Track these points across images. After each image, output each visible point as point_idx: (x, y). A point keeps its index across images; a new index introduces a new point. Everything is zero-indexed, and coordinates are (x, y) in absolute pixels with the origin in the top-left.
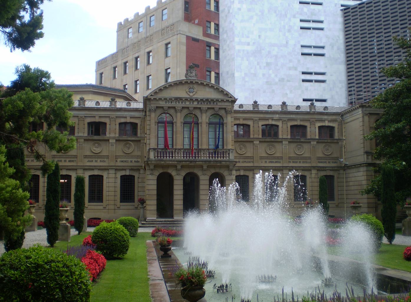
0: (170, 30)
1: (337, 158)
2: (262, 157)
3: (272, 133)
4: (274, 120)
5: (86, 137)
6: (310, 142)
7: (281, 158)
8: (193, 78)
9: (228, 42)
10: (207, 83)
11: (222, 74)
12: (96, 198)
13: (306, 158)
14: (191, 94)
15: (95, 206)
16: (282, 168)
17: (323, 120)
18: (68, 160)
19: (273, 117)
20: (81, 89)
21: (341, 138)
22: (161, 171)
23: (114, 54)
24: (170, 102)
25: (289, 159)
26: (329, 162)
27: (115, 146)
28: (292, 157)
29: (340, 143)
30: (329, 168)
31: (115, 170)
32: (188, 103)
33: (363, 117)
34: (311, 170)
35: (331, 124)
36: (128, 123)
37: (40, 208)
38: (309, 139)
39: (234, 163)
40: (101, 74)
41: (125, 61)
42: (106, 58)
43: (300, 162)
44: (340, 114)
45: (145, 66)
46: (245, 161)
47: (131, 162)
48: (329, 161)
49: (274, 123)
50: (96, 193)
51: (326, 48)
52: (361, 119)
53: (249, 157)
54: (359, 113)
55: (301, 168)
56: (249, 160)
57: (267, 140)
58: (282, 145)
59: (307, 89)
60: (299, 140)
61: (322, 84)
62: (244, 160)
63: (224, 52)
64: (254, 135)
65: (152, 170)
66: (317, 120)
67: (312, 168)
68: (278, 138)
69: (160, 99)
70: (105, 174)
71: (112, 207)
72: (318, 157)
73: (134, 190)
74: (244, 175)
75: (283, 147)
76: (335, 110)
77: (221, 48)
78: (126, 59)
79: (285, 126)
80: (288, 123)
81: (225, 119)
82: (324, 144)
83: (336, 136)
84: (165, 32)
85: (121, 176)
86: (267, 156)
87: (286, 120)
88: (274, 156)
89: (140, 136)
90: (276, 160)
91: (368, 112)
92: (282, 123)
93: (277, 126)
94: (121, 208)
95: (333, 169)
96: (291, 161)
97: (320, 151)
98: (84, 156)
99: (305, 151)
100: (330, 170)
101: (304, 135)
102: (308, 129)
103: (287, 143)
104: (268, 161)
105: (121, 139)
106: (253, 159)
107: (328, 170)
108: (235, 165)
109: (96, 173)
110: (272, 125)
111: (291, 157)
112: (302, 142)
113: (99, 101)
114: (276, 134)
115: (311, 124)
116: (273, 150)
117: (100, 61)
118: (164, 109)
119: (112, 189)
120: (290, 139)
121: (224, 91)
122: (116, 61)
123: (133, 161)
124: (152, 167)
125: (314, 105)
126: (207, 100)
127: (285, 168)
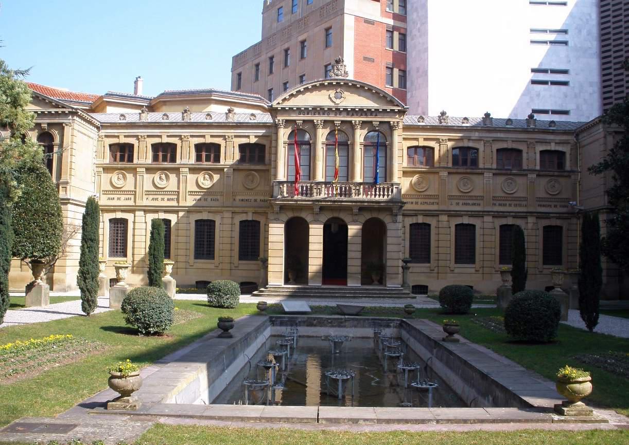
0: (331, 8)
1: (568, 200)
4: (472, 140)
6: (526, 175)
7: (482, 198)
8: (340, 77)
9: (419, 25)
10: (361, 84)
11: (409, 71)
12: (205, 252)
14: (338, 101)
16: (481, 213)
17: (548, 141)
18: (166, 197)
20: (198, 97)
21: (574, 169)
22: (290, 215)
23: (256, 45)
24: (306, 114)
25: (493, 200)
26: (555, 206)
27: (232, 178)
28: (498, 197)
29: (573, 177)
30: (555, 215)
33: (605, 137)
34: (527, 218)
35: (560, 148)
36: (421, 147)
37: (432, 272)
38: (524, 170)
39: (400, 204)
40: (240, 75)
41: (270, 55)
42: (245, 51)
43: (510, 205)
44: (574, 133)
45: (297, 61)
46: (425, 203)
47: (417, 203)
48: (556, 203)
49: (471, 144)
50: (205, 246)
51: (570, 32)
52: (602, 141)
54: (599, 131)
55: (512, 214)
56: (432, 201)
57: (460, 171)
58: (484, 179)
59: (538, 95)
60: (509, 172)
61: (563, 88)
63: (412, 39)
64: (484, 164)
65: (277, 213)
66: (539, 142)
67: (528, 214)
69: (291, 109)
70: (217, 219)
72: (537, 198)
73: (259, 243)
74: (253, 221)
75: (485, 182)
76: (570, 126)
77: (408, 33)
78: (271, 52)
79: (488, 150)
80: (493, 146)
81: (389, 138)
82: (547, 179)
83: (568, 166)
84: (325, 11)
85: (241, 222)
86: (111, 189)
87: (533, 142)
89: (438, 166)
91: (613, 130)
92: (484, 146)
94: (195, 267)
95: (560, 216)
96: (497, 203)
97: (542, 186)
99: (520, 187)
100: (557, 218)
101: (519, 164)
102: (525, 155)
103: (491, 175)
104: (461, 202)
105: (241, 167)
106: (178, 195)
107: (553, 217)
108: (401, 207)
109: (466, 220)
110: (469, 148)
111: (496, 197)
112: (514, 175)
114: (475, 162)
115: (528, 147)
116: (469, 186)
117: (237, 56)
118: (296, 123)
119: (228, 240)
120: (496, 169)
121: (386, 95)
122: (259, 55)
123: (258, 200)
124: (277, 209)
125: (491, 117)
126: (361, 110)
127: (486, 213)
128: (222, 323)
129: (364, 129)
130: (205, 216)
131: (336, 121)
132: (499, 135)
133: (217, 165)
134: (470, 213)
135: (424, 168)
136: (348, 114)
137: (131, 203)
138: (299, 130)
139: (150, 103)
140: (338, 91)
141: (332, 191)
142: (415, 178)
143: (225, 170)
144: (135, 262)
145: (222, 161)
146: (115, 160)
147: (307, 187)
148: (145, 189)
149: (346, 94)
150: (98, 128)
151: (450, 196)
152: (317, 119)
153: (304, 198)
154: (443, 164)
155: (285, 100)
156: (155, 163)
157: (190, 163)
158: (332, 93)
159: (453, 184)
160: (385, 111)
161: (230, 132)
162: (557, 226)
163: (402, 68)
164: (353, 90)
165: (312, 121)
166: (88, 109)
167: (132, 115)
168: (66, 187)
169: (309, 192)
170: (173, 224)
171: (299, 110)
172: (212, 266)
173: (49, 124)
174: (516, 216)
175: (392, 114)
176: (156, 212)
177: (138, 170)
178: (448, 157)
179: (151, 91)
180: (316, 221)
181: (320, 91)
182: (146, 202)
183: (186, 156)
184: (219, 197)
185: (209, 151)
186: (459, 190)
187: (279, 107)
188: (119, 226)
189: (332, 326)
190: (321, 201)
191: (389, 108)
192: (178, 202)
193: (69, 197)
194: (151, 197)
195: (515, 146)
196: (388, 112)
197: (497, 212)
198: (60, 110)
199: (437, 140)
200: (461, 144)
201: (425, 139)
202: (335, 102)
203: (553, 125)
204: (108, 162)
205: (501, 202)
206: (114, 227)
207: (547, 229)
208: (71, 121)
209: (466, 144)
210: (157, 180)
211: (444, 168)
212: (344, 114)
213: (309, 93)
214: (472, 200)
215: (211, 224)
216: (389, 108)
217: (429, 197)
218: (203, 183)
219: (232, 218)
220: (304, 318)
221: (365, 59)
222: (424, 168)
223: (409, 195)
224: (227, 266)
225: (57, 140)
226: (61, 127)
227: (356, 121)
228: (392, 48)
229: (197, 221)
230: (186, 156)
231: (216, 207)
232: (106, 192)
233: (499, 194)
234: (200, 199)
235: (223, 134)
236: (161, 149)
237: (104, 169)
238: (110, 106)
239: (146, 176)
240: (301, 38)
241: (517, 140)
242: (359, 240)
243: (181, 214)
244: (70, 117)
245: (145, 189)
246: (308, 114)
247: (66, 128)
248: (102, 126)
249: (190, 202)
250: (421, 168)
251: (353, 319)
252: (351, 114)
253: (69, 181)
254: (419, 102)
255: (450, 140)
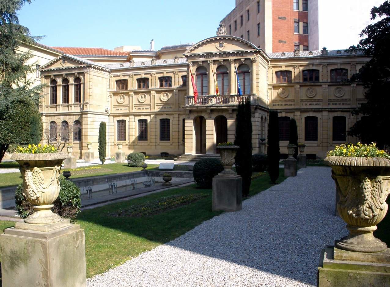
2: (302, 100)
3: (314, 77)
4: (315, 65)
5: (329, 82)
7: (321, 100)
8: (222, 35)
13: (345, 100)
14: (221, 49)
15: (308, 144)
18: (145, 107)
19: (313, 63)
22: (196, 115)
23: (234, 9)
31: (179, 114)
32: (218, 57)
41: (234, 20)
43: (340, 104)
47: (282, 105)
49: (314, 68)
50: (166, 133)
53: (291, 100)
55: (340, 110)
56: (291, 103)
62: (286, 103)
63: (311, 3)
68: (319, 82)
69: (195, 55)
71: (154, 144)
79: (325, 71)
81: (250, 68)
86: (118, 104)
88: (343, 98)
90: (317, 103)
93: (318, 71)
98: (300, 100)
103: (327, 86)
104: (308, 103)
105: (182, 89)
106: (151, 106)
109: (311, 114)
110: (313, 70)
113: (166, 60)
114: (317, 79)
115: (351, 67)
119: (177, 130)
125: (326, 50)
126: (233, 53)
128: (66, 174)
129: (215, 65)
130: (164, 117)
131: (200, 61)
132: (332, 61)
133: (170, 89)
134: (313, 110)
135: (285, 84)
136: (226, 56)
137: (127, 111)
138: (242, 64)
139: (157, 54)
140: (221, 42)
141: (219, 100)
142: (280, 90)
143: (174, 91)
144: (130, 143)
145: (173, 86)
146: (119, 89)
147: (203, 99)
148: (134, 104)
149: (225, 44)
150: (109, 72)
151: (329, 99)
152: (210, 60)
153: (201, 105)
154: (297, 81)
155: (191, 50)
156: (139, 89)
157: (156, 88)
158: (217, 44)
159: (304, 93)
160: (247, 52)
161: (176, 70)
162: (167, 119)
163: (305, 21)
164: (229, 41)
165: (207, 61)
166: (127, 60)
167: (148, 62)
168: (87, 105)
169: (204, 102)
170: (148, 121)
171: (199, 56)
172: (169, 144)
173: (78, 73)
174: (315, 111)
175: (246, 54)
176: (140, 115)
177: (130, 93)
178: (300, 76)
179: (156, 48)
180: (210, 118)
181: (206, 45)
182: (135, 110)
183: (155, 84)
184: (172, 106)
185: (165, 81)
186: (307, 96)
187: (189, 55)
188: (122, 124)
189: (177, 177)
190: (210, 107)
191: (249, 50)
192: (151, 110)
193: (88, 110)
194: (137, 108)
195: (342, 67)
196: (249, 53)
197: (331, 109)
198: (82, 66)
199: (293, 66)
200: (308, 68)
201: (286, 66)
202: (218, 49)
203: (339, 53)
204: (115, 90)
205: (333, 103)
206: (141, 124)
207: (335, 119)
208: (88, 71)
209: (311, 68)
210: (162, 97)
211: (297, 83)
212: (224, 55)
213: (205, 46)
214: (315, 102)
215: (168, 121)
216: (249, 50)
217: (290, 101)
218: (163, 99)
219: (179, 117)
220: (163, 172)
221: (280, 18)
222: (285, 84)
223: (277, 100)
224: (177, 144)
225: (83, 81)
226: (83, 74)
227: (231, 59)
228: (298, 10)
229: (161, 120)
230: (155, 84)
231: (171, 112)
232: (115, 106)
233: (333, 97)
234: (162, 108)
235: (173, 71)
236: (142, 81)
237: (113, 94)
238: (134, 57)
239: (134, 96)
240: (247, 9)
241: (344, 63)
242: (234, 128)
243: (152, 116)
244: (88, 69)
245: (134, 104)
246: (205, 57)
247: (86, 75)
248: (111, 71)
249: (157, 109)
250: (283, 84)
251: (188, 173)
252: (228, 55)
253: (88, 102)
254: (314, 42)
255: (301, 66)
